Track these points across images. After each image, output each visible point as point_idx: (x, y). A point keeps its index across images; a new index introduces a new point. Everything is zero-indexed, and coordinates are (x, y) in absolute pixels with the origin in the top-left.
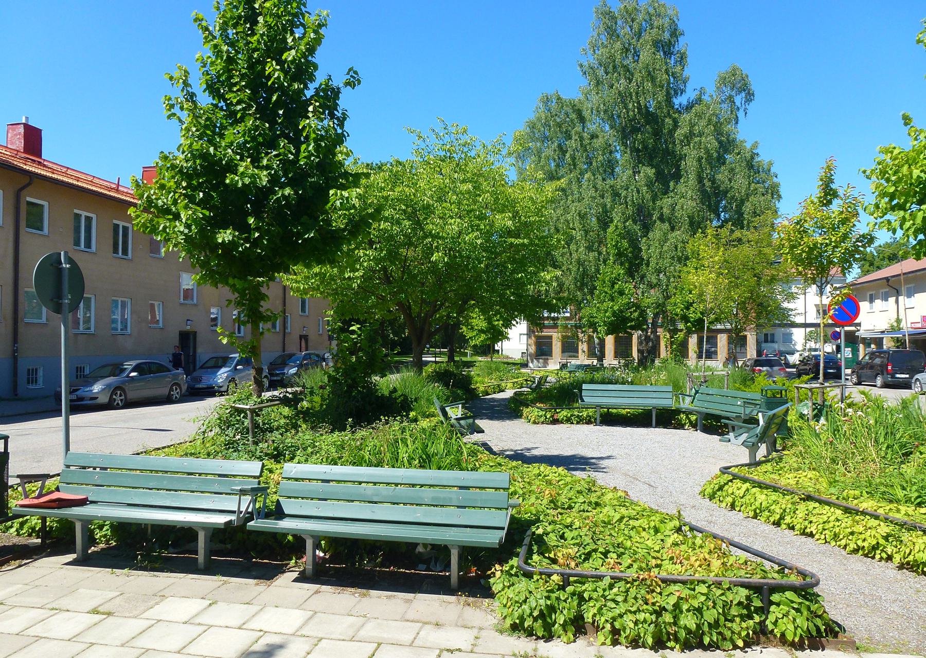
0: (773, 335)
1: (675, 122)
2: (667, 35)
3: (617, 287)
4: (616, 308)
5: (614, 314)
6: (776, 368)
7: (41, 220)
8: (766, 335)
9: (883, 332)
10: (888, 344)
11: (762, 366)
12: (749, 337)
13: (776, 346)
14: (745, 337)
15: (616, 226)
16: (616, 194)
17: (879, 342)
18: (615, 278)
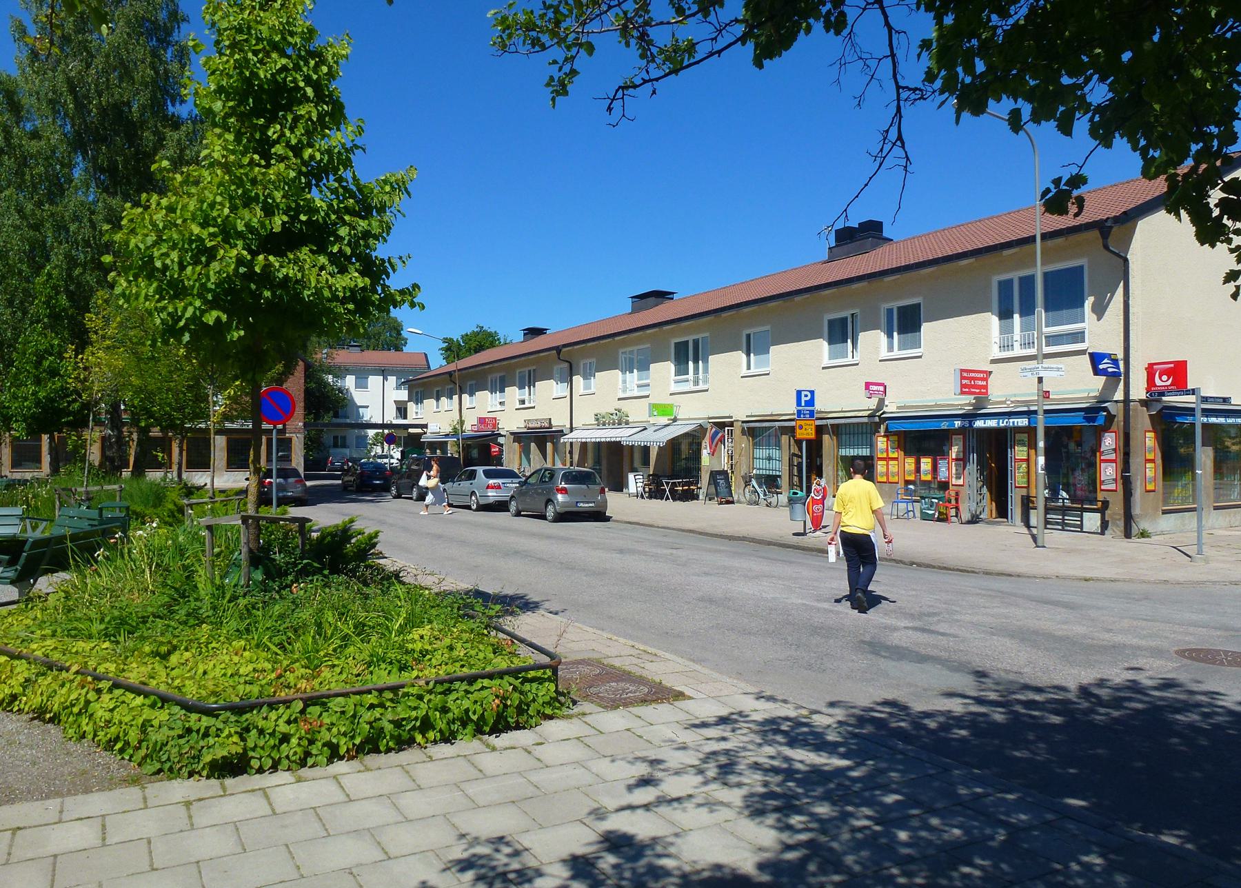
0: (344, 438)
1: (161, 138)
2: (162, 16)
3: (46, 364)
4: (42, 395)
5: (38, 403)
6: (291, 480)
7: (1076, 268)
8: (336, 438)
9: (447, 436)
10: (451, 451)
11: (1048, 453)
12: (295, 440)
13: (347, 451)
14: (290, 439)
15: (49, 275)
16: (61, 227)
17: (443, 446)
18: (46, 351)
